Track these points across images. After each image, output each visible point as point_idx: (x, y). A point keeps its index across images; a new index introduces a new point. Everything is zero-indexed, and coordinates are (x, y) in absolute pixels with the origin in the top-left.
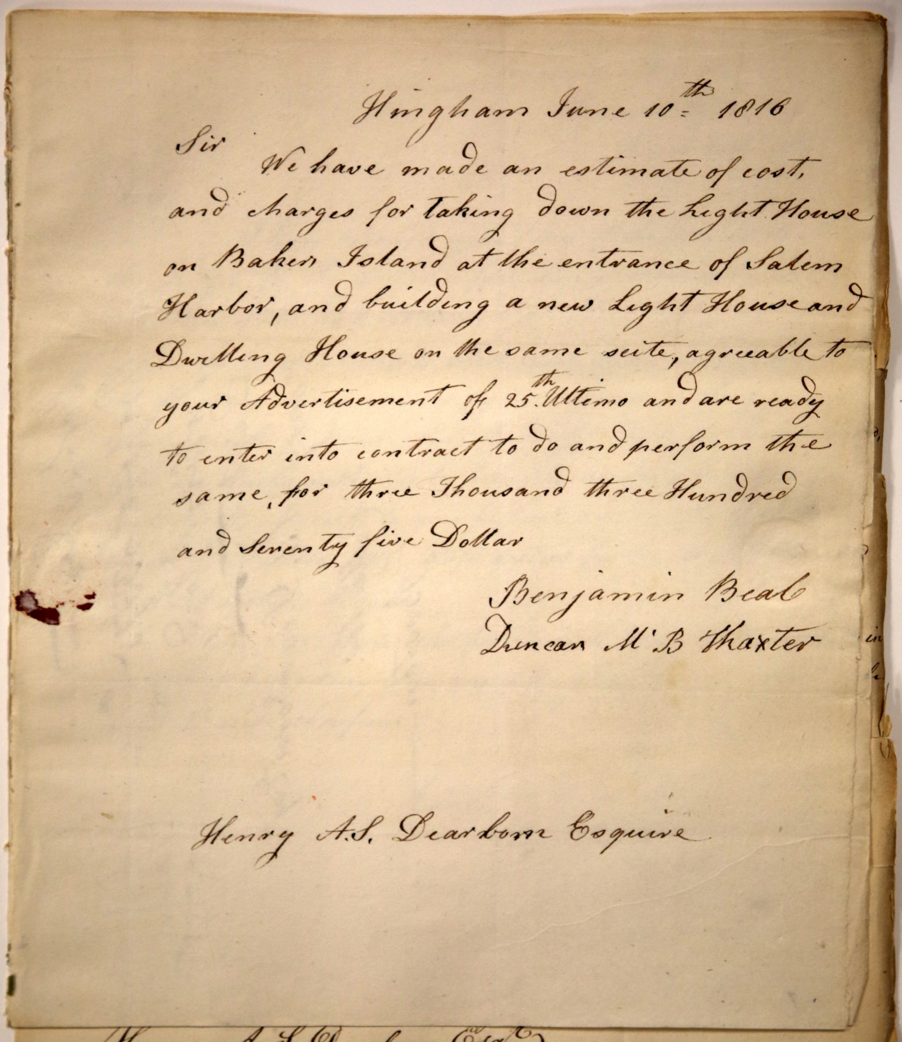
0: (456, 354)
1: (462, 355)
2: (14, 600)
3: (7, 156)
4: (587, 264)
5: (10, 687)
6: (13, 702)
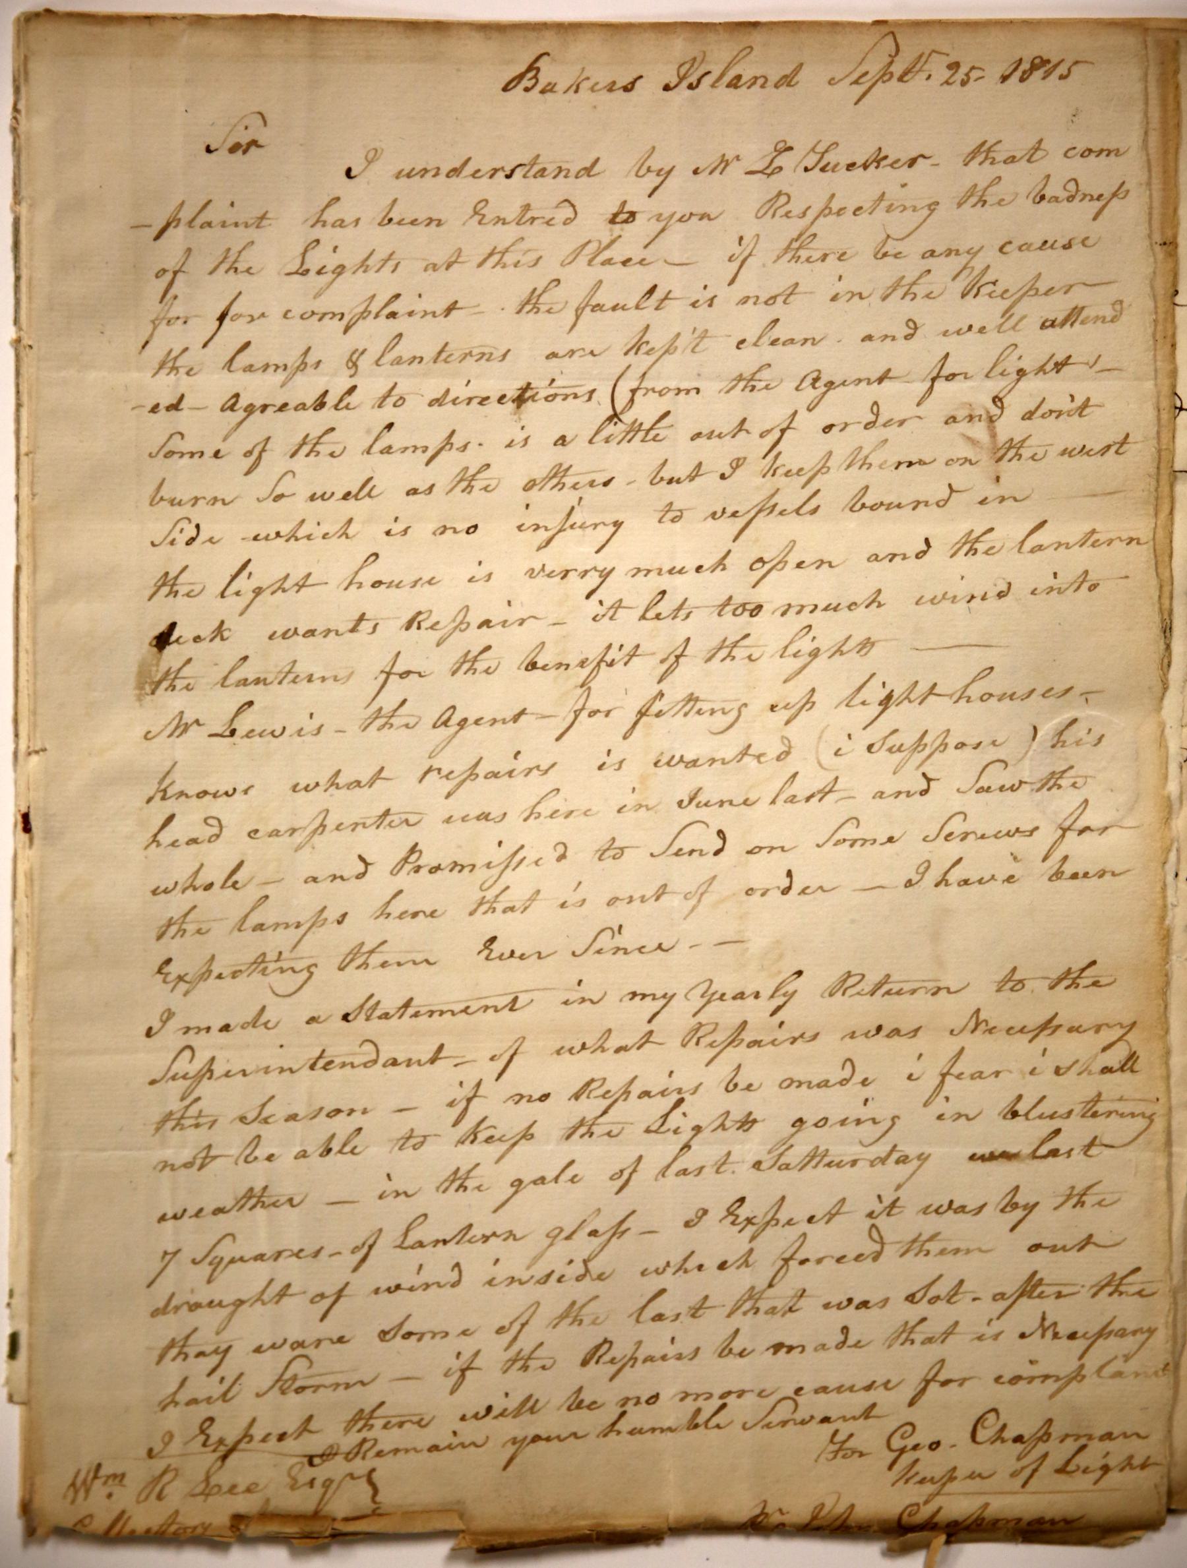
0: (126, 1517)
1: (896, 1346)
2: (20, 819)
3: (13, 211)
4: (923, 600)
5: (14, 938)
6: (18, 958)
